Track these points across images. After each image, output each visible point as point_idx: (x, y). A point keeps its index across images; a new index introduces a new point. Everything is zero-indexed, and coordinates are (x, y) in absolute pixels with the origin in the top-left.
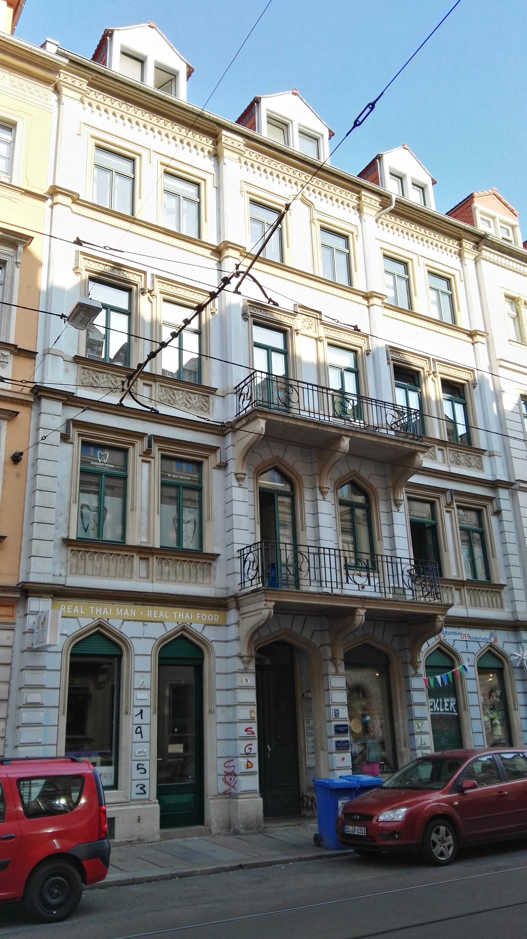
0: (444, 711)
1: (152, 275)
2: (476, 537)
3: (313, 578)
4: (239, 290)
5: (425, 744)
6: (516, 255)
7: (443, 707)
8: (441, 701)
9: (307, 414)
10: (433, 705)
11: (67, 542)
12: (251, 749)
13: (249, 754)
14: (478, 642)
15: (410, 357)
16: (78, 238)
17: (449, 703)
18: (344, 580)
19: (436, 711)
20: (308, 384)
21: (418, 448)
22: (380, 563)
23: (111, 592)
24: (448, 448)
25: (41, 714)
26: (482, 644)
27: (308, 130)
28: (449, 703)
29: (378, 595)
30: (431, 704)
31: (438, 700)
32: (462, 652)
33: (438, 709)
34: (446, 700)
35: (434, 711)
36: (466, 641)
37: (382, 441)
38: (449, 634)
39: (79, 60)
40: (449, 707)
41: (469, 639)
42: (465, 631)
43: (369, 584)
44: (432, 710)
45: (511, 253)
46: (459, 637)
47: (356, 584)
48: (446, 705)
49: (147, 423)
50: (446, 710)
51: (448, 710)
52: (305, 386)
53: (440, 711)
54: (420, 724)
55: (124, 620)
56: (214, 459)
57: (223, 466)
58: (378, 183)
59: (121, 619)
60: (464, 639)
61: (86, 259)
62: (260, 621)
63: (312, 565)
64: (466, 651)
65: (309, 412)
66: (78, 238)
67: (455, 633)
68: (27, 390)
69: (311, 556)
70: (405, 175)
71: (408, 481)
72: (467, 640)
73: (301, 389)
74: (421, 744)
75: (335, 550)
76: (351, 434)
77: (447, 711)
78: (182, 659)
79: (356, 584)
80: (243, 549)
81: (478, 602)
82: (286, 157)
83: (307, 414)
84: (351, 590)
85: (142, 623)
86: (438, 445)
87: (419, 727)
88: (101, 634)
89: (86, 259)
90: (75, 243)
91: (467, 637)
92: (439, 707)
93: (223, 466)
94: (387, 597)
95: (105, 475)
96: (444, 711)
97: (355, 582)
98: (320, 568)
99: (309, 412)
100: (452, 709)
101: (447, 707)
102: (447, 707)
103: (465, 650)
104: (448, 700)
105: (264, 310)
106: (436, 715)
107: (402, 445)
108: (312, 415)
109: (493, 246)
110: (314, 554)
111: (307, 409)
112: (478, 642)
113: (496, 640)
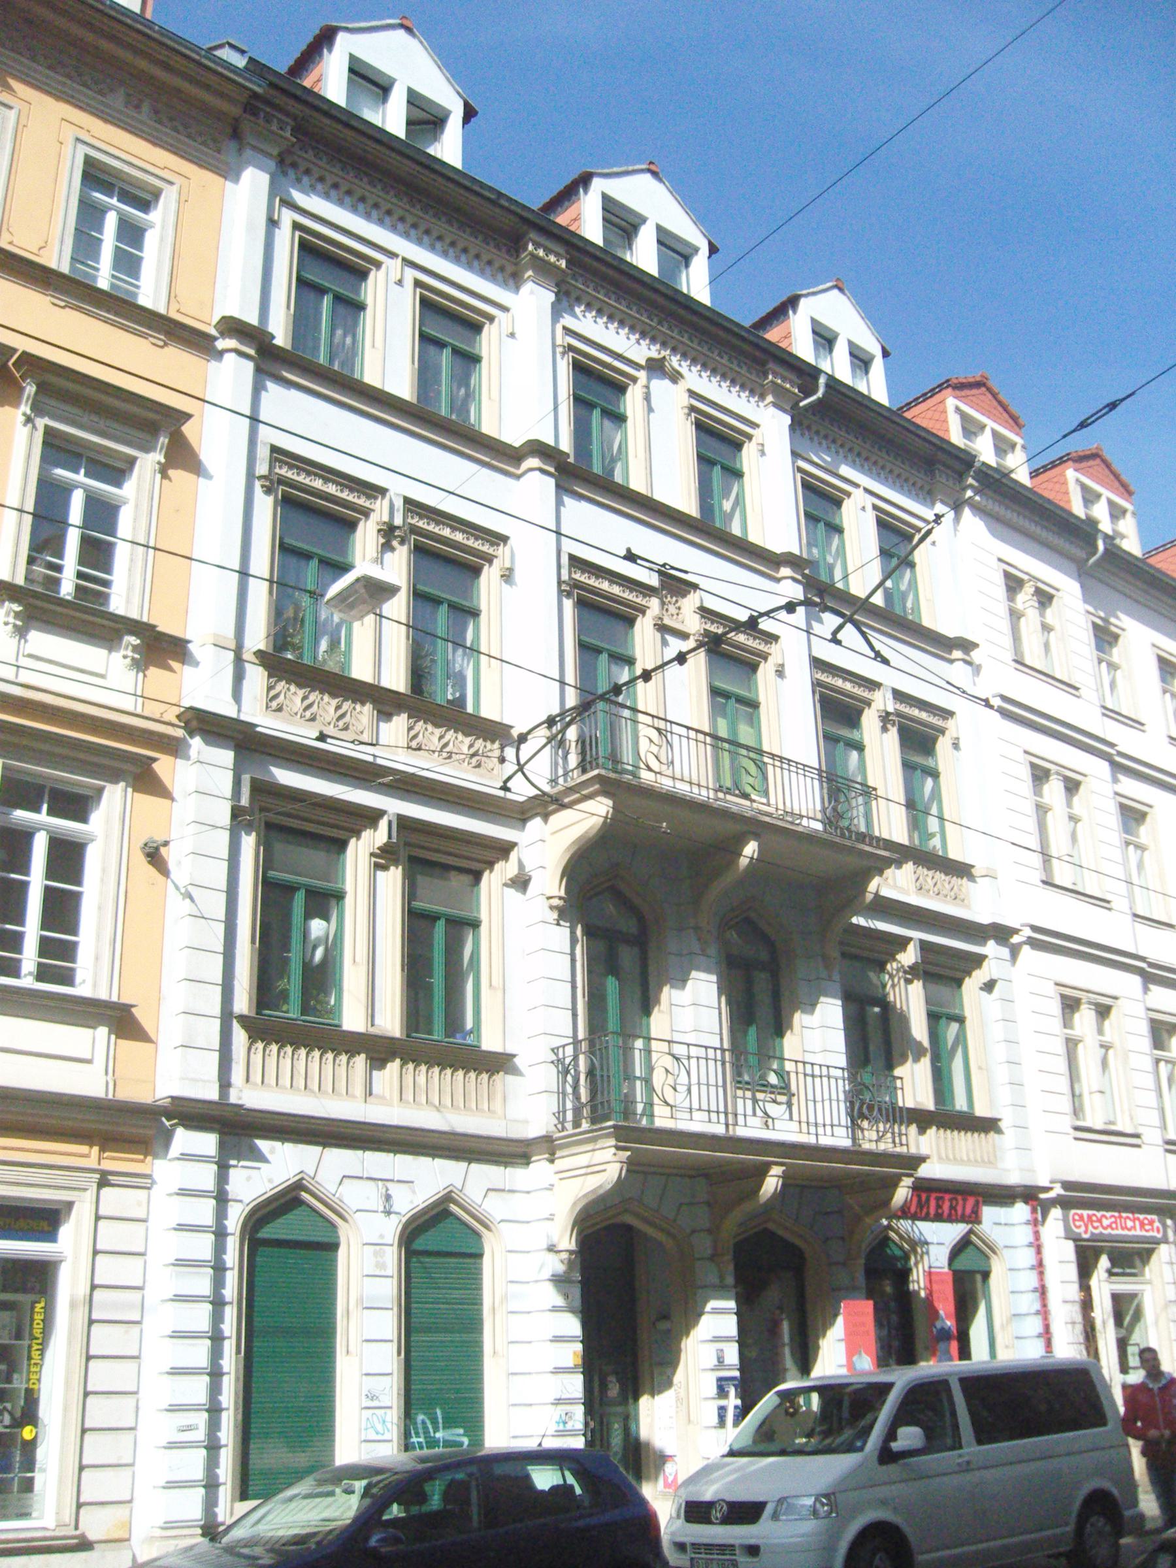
1: (274, 449)
3: (695, 1105)
4: (839, 636)
9: (686, 787)
16: (629, 550)
18: (749, 1111)
20: (688, 728)
23: (193, 1104)
29: (720, 1130)
43: (791, 1119)
47: (668, 1104)
52: (683, 731)
56: (506, 869)
57: (521, 883)
59: (330, 1170)
62: (601, 1186)
63: (694, 1080)
65: (691, 783)
66: (629, 550)
68: (171, 715)
69: (693, 1061)
70: (392, 82)
73: (676, 738)
75: (715, 1049)
78: (439, 1249)
79: (668, 1104)
80: (564, 1046)
81: (341, 1085)
83: (686, 787)
84: (751, 1129)
88: (289, 1199)
90: (625, 558)
93: (521, 883)
94: (731, 1132)
97: (666, 1102)
99: (691, 783)
108: (695, 790)
110: (698, 1058)
111: (687, 778)
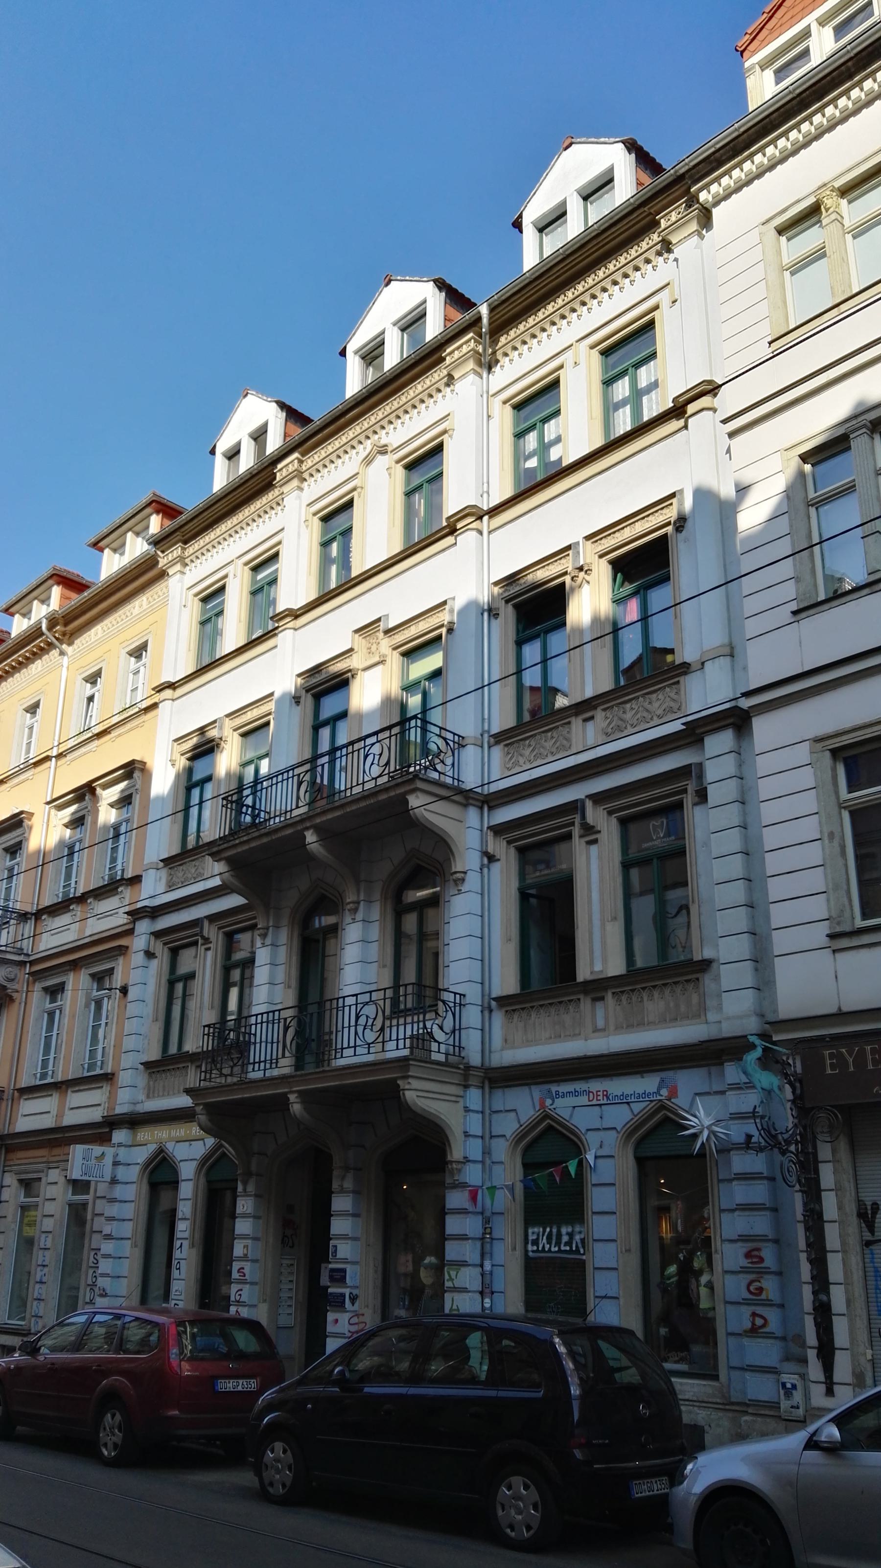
0: (560, 1251)
2: (659, 871)
5: (458, 1310)
6: (780, 116)
7: (558, 1243)
8: (555, 1230)
10: (538, 1239)
11: (147, 1065)
12: (240, 1295)
13: (238, 1301)
14: (628, 1103)
15: (338, 665)
17: (571, 1235)
19: (543, 1250)
21: (299, 828)
22: (328, 1013)
24: (599, 709)
25: (111, 1245)
26: (637, 1107)
27: (409, 317)
28: (571, 1235)
30: (535, 1237)
31: (548, 1230)
32: (588, 1130)
33: (547, 1247)
34: (564, 1230)
35: (537, 1251)
36: (600, 1105)
37: (348, 810)
38: (563, 1096)
39: (646, 193)
40: (569, 1243)
41: (605, 1102)
42: (596, 1085)
44: (535, 1248)
45: (802, 101)
46: (583, 1100)
48: (565, 1238)
49: (210, 902)
50: (563, 1248)
51: (568, 1248)
53: (550, 1251)
54: (453, 1274)
55: (574, 1107)
58: (180, 513)
59: (572, 1105)
60: (595, 1102)
61: (596, 541)
64: (598, 1126)
67: (576, 1094)
71: (246, 901)
72: (601, 1102)
74: (451, 1310)
76: (308, 824)
77: (555, 1252)
82: (343, 420)
85: (187, 1143)
86: (577, 714)
87: (451, 1279)
89: (596, 541)
91: (600, 1098)
92: (549, 1243)
95: (658, 858)
96: (560, 1251)
98: (272, 1043)
100: (577, 1246)
101: (566, 1244)
102: (566, 1244)
103: (597, 1125)
104: (570, 1230)
105: (318, 672)
106: (542, 1258)
107: (375, 800)
109: (714, 164)
112: (628, 1103)
113: (673, 1093)
